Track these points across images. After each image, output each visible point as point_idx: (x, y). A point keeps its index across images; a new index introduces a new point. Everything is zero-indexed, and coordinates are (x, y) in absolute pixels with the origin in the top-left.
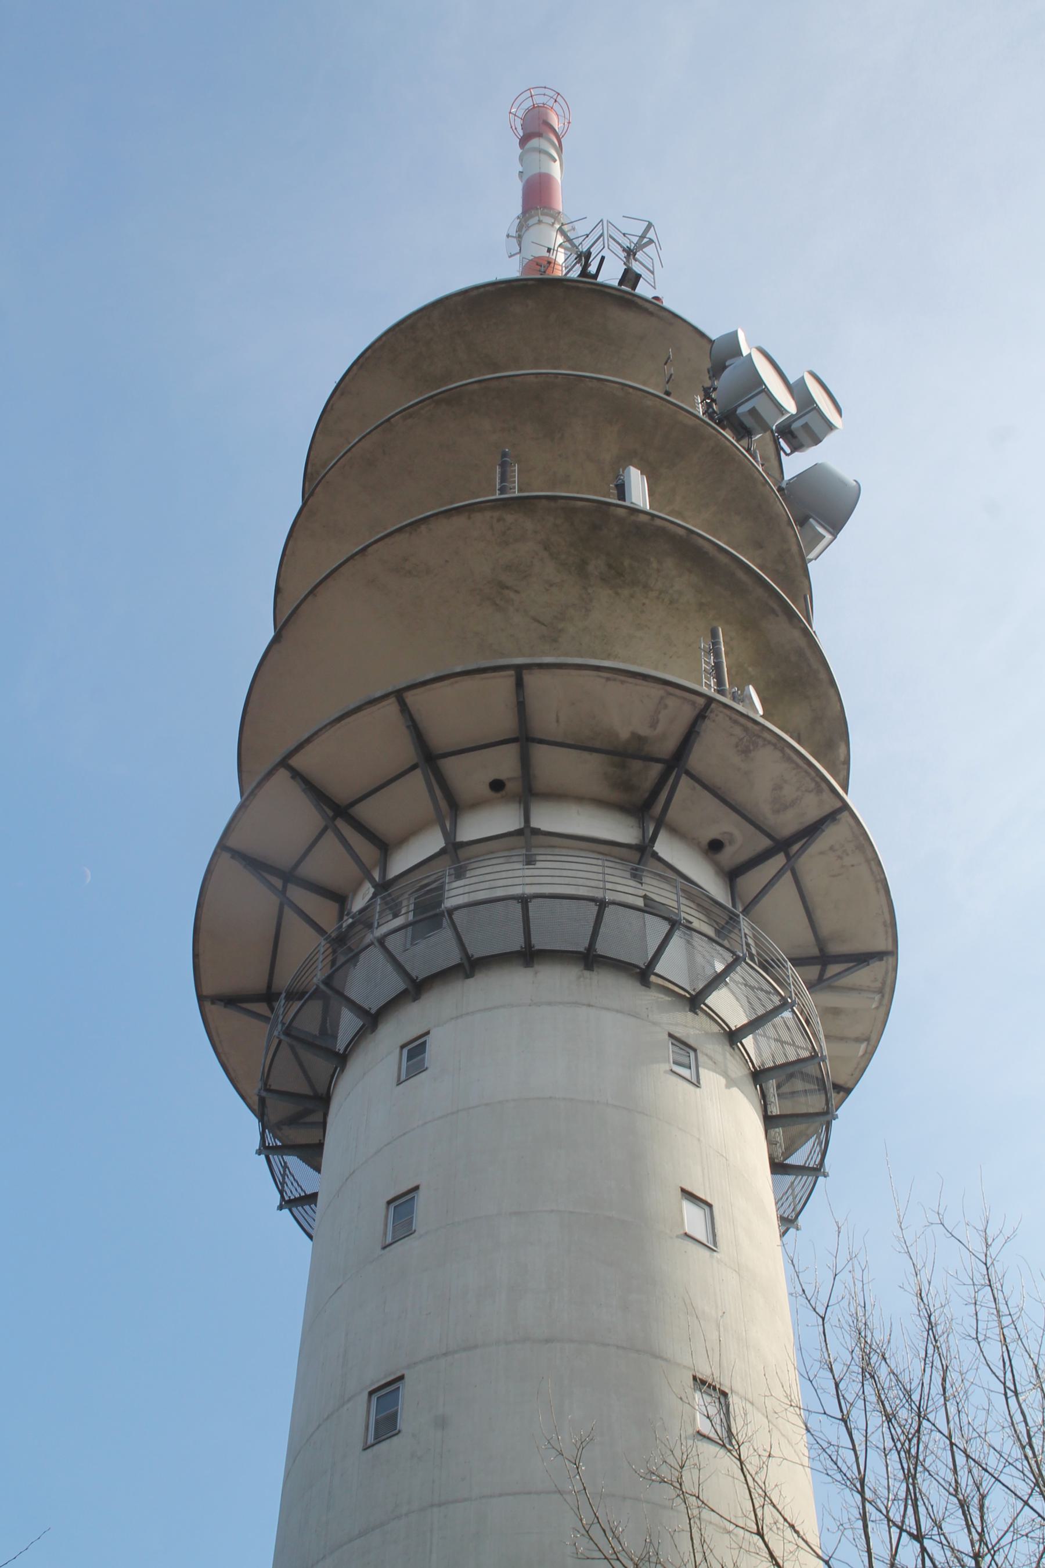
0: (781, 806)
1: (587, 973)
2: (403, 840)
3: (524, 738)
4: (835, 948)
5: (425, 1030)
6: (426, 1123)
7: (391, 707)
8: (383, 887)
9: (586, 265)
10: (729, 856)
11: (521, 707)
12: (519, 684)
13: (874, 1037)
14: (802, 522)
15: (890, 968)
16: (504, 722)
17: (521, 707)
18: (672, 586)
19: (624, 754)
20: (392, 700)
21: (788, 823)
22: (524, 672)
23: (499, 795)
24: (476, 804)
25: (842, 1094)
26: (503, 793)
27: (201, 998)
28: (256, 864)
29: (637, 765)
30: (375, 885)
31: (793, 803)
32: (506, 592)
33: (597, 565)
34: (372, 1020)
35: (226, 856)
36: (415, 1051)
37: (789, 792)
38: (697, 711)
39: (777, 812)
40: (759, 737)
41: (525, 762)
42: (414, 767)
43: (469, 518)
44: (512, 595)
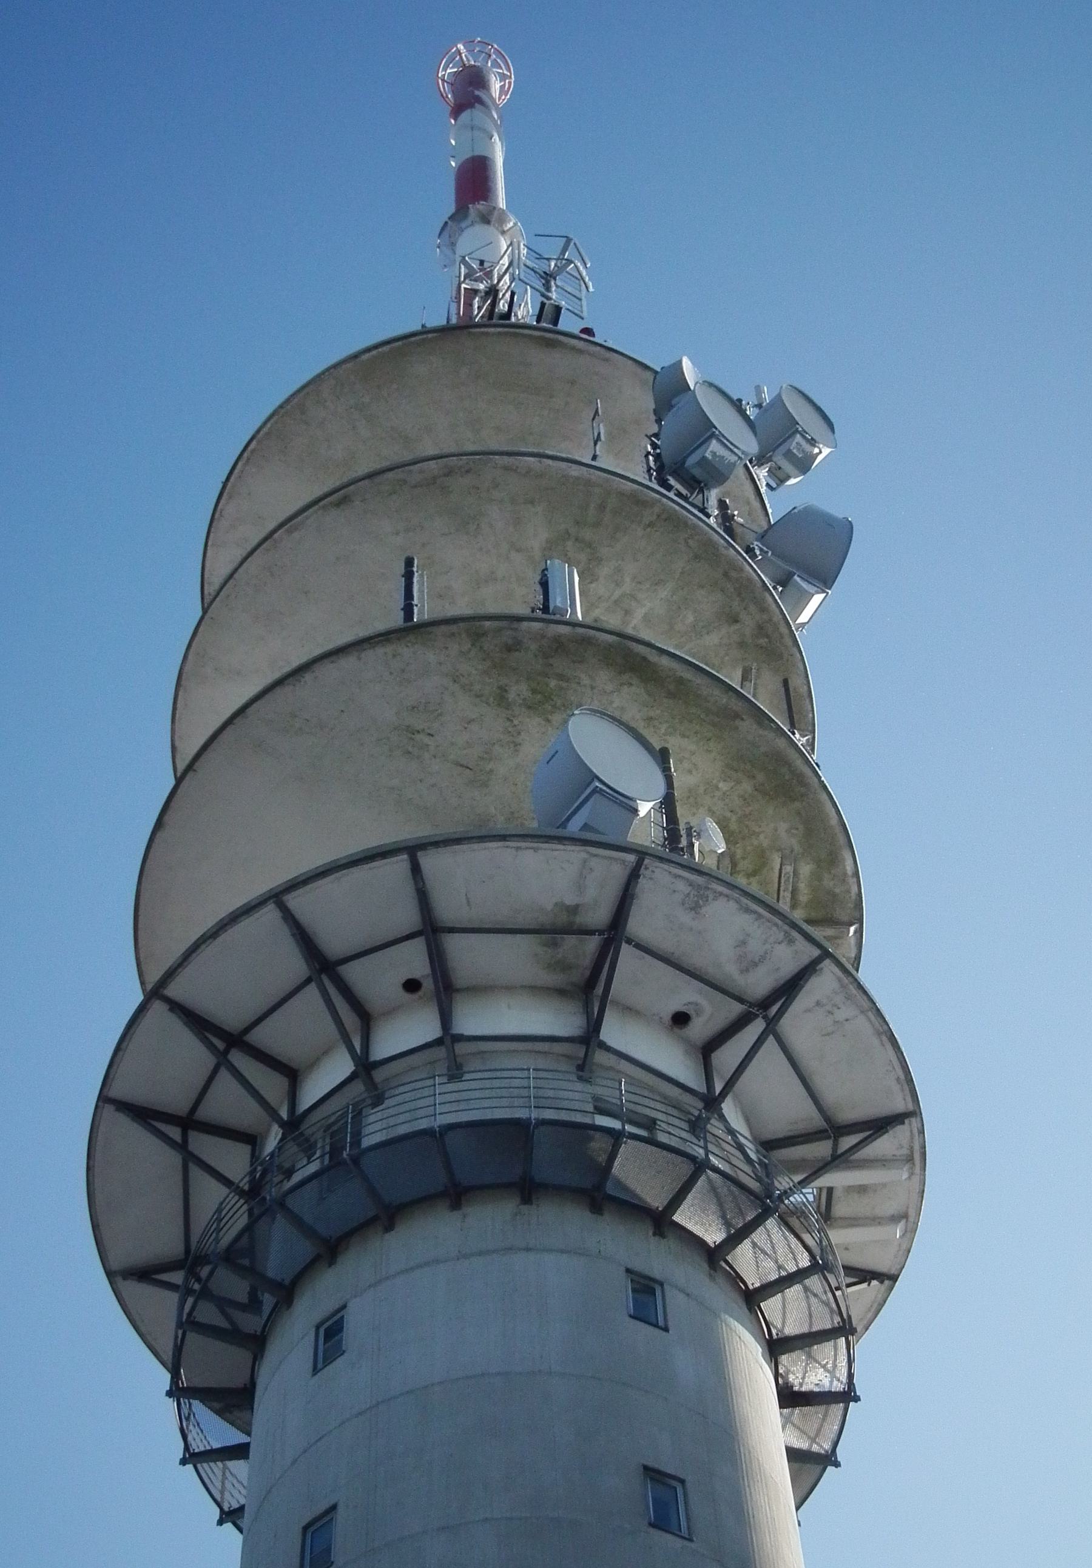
0: (749, 965)
1: (524, 1208)
2: (314, 1064)
3: (431, 930)
4: (848, 1115)
5: (341, 1303)
6: (343, 1423)
7: (270, 914)
8: (293, 1125)
9: (494, 304)
10: (700, 1029)
11: (423, 897)
12: (416, 869)
13: (912, 1213)
14: (784, 581)
15: (915, 1131)
16: (407, 917)
17: (423, 897)
18: (612, 702)
19: (554, 930)
20: (271, 907)
21: (760, 983)
22: (419, 854)
23: (415, 996)
24: (391, 1012)
25: (887, 1282)
26: (420, 993)
27: (110, 1274)
28: (144, 1115)
29: (571, 940)
30: (283, 1124)
31: (763, 958)
32: (418, 737)
33: (518, 690)
34: (287, 1293)
35: (109, 1110)
36: (331, 1334)
37: (755, 947)
38: (628, 872)
39: (745, 971)
40: (707, 888)
41: (437, 958)
42: (308, 981)
43: (359, 659)
44: (426, 740)
